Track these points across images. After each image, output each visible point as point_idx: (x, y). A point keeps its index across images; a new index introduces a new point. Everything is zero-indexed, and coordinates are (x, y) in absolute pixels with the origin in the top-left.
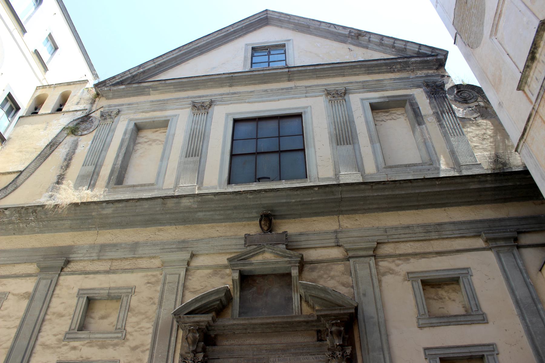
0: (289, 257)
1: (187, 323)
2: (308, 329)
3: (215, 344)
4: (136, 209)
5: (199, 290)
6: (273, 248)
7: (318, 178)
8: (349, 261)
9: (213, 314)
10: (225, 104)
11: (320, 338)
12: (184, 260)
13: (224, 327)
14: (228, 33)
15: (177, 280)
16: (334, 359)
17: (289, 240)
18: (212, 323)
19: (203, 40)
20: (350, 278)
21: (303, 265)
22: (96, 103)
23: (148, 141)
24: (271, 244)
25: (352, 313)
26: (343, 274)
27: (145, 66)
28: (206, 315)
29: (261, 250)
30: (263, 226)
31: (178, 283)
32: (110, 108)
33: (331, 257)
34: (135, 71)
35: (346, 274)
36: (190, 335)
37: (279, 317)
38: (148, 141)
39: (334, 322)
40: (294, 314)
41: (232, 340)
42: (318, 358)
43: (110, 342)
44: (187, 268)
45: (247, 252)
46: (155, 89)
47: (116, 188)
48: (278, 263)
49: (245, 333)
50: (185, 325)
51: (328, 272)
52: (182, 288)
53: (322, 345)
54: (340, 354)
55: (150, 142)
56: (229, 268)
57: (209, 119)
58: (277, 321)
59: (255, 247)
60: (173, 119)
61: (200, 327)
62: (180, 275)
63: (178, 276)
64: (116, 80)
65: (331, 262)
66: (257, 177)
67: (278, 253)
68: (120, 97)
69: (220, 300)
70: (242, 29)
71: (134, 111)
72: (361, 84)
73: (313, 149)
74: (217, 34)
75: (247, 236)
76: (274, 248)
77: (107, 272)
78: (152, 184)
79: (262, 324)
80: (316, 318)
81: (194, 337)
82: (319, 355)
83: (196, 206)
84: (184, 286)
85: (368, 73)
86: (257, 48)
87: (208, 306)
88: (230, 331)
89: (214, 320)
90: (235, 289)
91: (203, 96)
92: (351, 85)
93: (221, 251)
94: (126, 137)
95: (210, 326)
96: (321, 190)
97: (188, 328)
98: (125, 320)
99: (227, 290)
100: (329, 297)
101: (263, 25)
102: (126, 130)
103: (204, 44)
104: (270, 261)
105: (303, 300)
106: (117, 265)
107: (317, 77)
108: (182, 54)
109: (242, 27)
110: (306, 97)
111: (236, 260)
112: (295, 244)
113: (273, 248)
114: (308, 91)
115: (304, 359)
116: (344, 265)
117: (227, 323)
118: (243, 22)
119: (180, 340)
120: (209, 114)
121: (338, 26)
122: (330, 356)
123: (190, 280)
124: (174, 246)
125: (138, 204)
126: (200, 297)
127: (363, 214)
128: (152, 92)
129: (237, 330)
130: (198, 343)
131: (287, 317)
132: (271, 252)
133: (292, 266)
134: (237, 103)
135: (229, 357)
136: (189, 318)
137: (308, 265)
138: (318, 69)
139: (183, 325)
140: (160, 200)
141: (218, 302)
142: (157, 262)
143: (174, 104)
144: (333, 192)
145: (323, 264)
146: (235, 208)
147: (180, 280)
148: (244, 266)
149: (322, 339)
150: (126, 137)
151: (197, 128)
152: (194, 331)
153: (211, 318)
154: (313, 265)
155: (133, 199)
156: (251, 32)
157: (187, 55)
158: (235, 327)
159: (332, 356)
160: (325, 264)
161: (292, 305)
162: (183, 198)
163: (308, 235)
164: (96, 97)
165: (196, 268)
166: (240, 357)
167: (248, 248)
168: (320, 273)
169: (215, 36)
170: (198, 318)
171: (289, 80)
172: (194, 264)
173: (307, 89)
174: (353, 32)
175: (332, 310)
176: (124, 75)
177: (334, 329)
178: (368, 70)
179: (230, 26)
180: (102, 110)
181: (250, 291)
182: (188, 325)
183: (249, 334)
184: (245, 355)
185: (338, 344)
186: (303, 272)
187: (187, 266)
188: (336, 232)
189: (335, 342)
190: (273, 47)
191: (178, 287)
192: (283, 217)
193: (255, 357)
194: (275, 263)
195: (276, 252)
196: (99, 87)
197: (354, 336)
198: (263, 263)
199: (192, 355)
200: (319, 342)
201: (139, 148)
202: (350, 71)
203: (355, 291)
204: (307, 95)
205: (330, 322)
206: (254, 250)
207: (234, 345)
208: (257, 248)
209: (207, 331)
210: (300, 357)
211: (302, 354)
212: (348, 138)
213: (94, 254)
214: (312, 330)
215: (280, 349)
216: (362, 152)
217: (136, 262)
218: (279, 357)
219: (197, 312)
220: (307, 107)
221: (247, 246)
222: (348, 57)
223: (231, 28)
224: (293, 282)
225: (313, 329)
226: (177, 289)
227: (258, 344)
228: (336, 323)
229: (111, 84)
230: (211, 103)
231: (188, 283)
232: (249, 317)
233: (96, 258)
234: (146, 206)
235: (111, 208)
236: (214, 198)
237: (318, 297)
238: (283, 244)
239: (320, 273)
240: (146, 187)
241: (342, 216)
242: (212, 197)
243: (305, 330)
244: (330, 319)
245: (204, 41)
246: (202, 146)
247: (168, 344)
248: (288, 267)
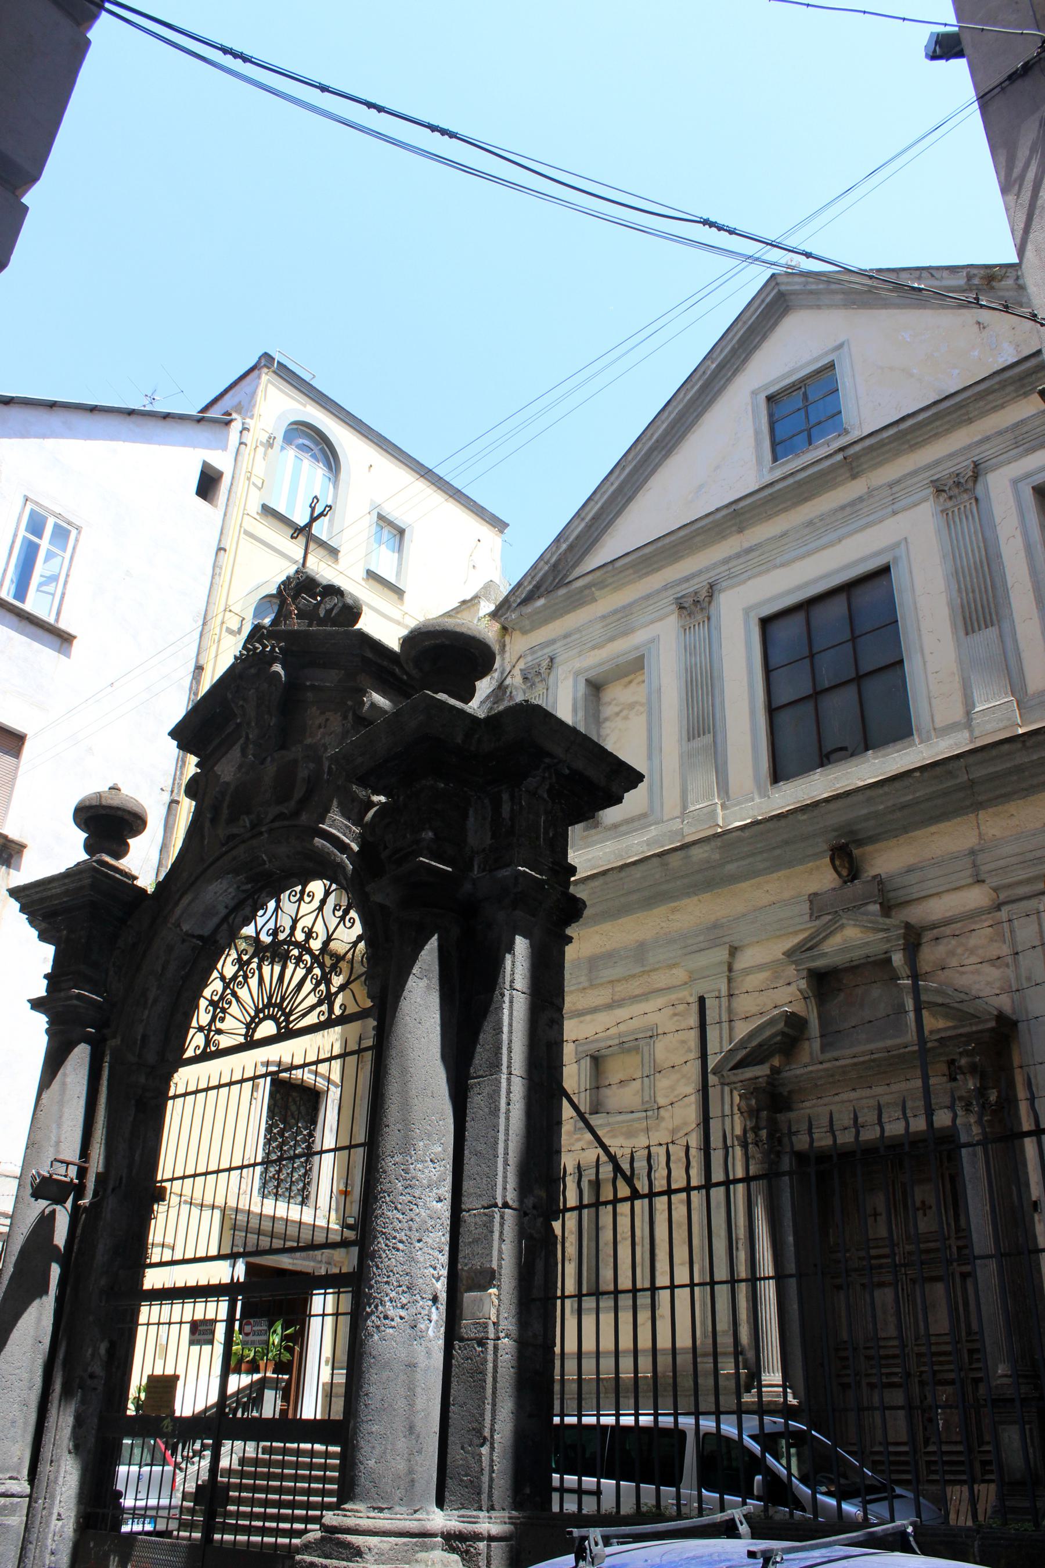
4: (623, 884)
7: (935, 729)
10: (740, 584)
12: (720, 963)
14: (707, 379)
19: (660, 422)
22: (507, 648)
23: (621, 711)
26: (992, 940)
27: (567, 533)
30: (840, 869)
32: (535, 656)
33: (968, 908)
34: (552, 555)
35: (996, 941)
38: (621, 711)
43: (637, 1125)
46: (601, 585)
47: (587, 837)
55: (625, 713)
57: (714, 632)
59: (830, 917)
60: (649, 649)
61: (758, 1086)
64: (524, 588)
66: (824, 752)
68: (546, 621)
69: (783, 1033)
70: (734, 352)
71: (579, 649)
72: (1009, 436)
73: (919, 655)
74: (683, 392)
75: (813, 898)
77: (609, 1007)
78: (644, 816)
81: (749, 1106)
83: (717, 856)
85: (1024, 393)
86: (779, 394)
91: (693, 576)
92: (987, 446)
93: (778, 933)
94: (578, 718)
96: (926, 774)
98: (652, 1087)
101: (779, 317)
102: (575, 700)
103: (665, 430)
106: (623, 990)
107: (911, 446)
108: (631, 474)
109: (733, 348)
110: (895, 513)
111: (798, 953)
112: (901, 892)
114: (897, 495)
118: (730, 336)
120: (713, 620)
121: (938, 268)
124: (701, 938)
125: (623, 874)
127: (1024, 798)
128: (597, 593)
132: (855, 925)
134: (760, 574)
138: (906, 429)
140: (655, 860)
142: (680, 975)
143: (645, 610)
144: (950, 772)
146: (786, 843)
150: (578, 718)
151: (696, 664)
155: (612, 869)
156: (756, 347)
157: (641, 471)
162: (693, 847)
163: (921, 869)
164: (503, 636)
169: (682, 400)
170: (749, 1073)
171: (854, 477)
172: (739, 965)
173: (895, 489)
174: (975, 276)
176: (536, 571)
178: (1023, 386)
179: (705, 358)
180: (521, 665)
181: (836, 1001)
188: (972, 852)
190: (810, 377)
192: (872, 840)
196: (502, 616)
198: (842, 950)
201: (608, 731)
202: (982, 403)
204: (896, 507)
212: (987, 610)
213: (583, 979)
216: (1019, 636)
217: (649, 980)
220: (896, 545)
222: (976, 353)
223: (709, 362)
229: (519, 600)
230: (712, 590)
233: (586, 984)
234: (638, 876)
235: (584, 890)
236: (742, 834)
238: (875, 902)
240: (636, 824)
241: (984, 812)
242: (739, 833)
245: (663, 422)
246: (713, 706)
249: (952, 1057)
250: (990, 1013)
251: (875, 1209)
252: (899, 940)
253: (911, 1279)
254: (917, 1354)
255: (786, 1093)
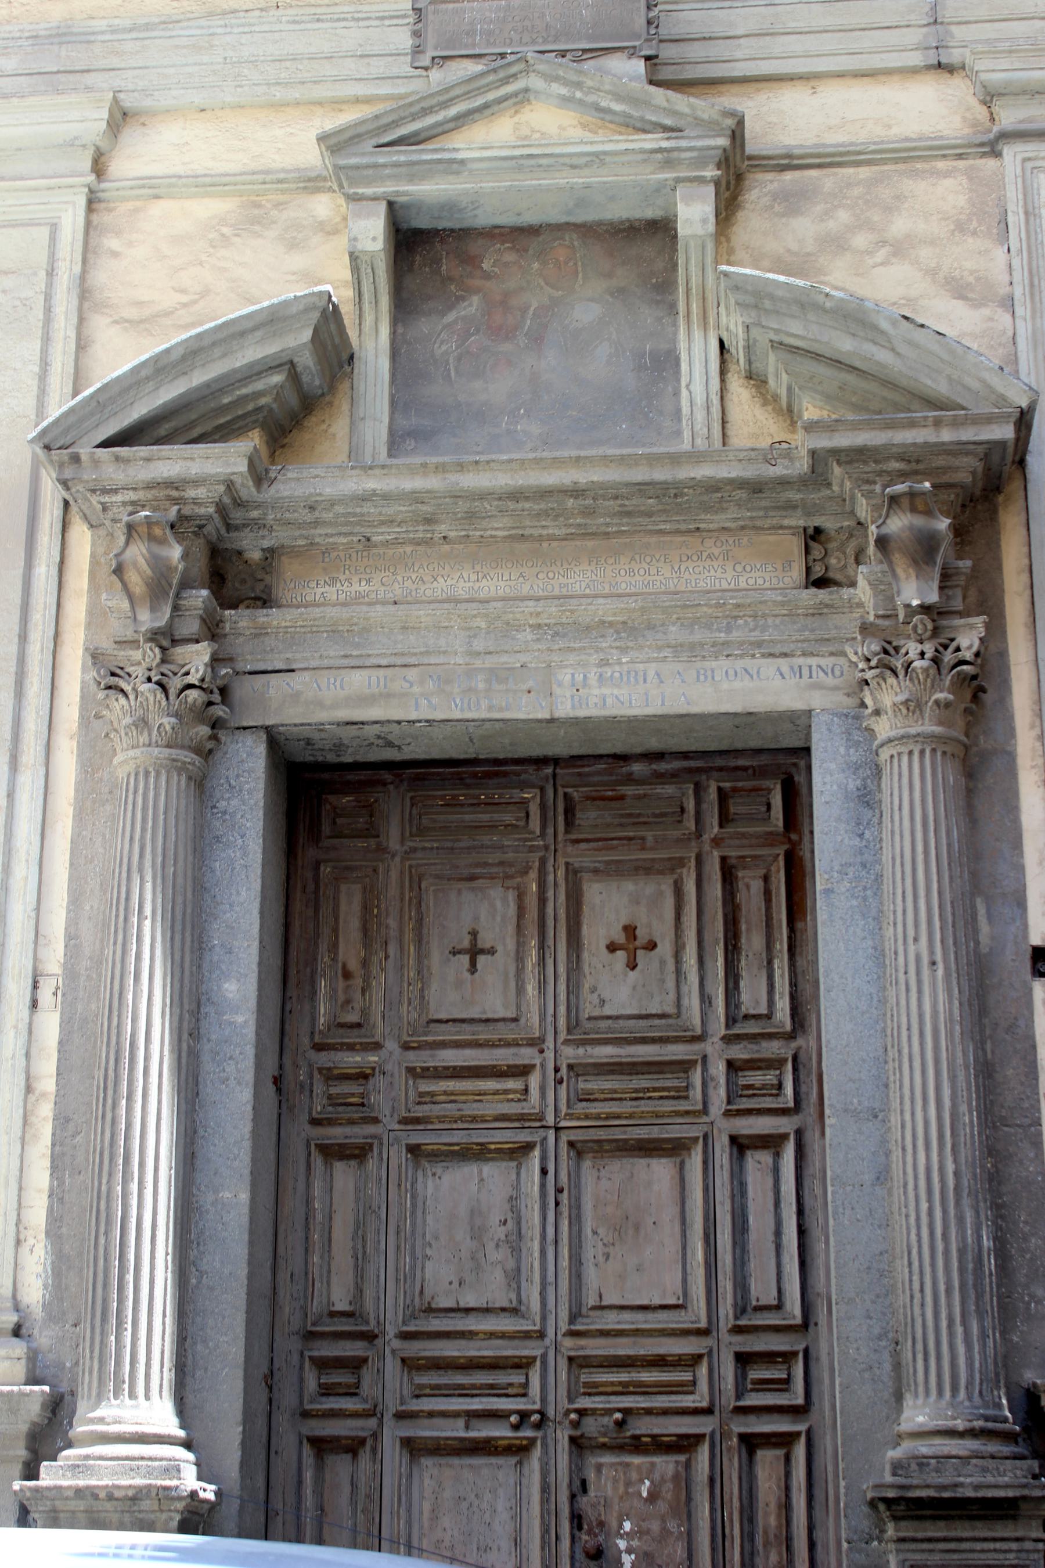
0: (666, 129)
1: (115, 491)
2: (759, 523)
3: (265, 601)
5: (168, 314)
6: (573, 77)
8: (997, 154)
9: (253, 441)
11: (818, 571)
12: (72, 144)
13: (312, 508)
15: (43, 259)
16: (892, 680)
17: (663, 32)
18: (247, 490)
20: (1000, 253)
21: (739, 177)
24: (563, 54)
25: (1002, 444)
26: (960, 227)
28: (216, 448)
29: (509, 89)
31: (51, 273)
33: (896, 131)
35: (974, 233)
36: (138, 553)
37: (606, 460)
39: (900, 488)
40: (686, 446)
41: (355, 579)
42: (805, 672)
44: (91, 191)
45: (432, 95)
48: (603, 163)
49: (427, 542)
50: (106, 499)
51: (876, 218)
52: (75, 302)
53: (827, 606)
54: (922, 654)
56: (330, 189)
58: (595, 479)
59: (474, 67)
61: (187, 511)
62: (54, 229)
63: (45, 231)
65: (896, 161)
67: (603, 104)
76: (581, 72)
79: (516, 495)
80: (802, 465)
82: (812, 654)
84: (84, 292)
87: (226, 401)
88: (344, 529)
89: (259, 477)
90: (366, 306)
93: (279, 93)
95: (239, 503)
97: (126, 519)
99: (324, 311)
100: (883, 356)
104: (557, 150)
105: (732, 367)
111: (368, 145)
112: (695, 51)
113: (573, 77)
115: (731, 672)
116: (970, 179)
117: (328, 491)
119: (79, 580)
122: (873, 663)
123: (115, 254)
126: (181, 351)
129: (383, 523)
130: (177, 596)
131: (653, 460)
132: (566, 101)
133: (678, 180)
135: (346, 662)
136: (127, 461)
137: (769, 176)
139: (94, 499)
141: (277, 379)
145: (850, 171)
147: (60, 255)
148: (411, 179)
149: (831, 574)
152: (157, 531)
153: (246, 462)
154: (797, 174)
158: (368, 508)
159: (881, 665)
160: (864, 172)
161: (677, 394)
165: (143, 187)
166: (399, 661)
167: (435, 75)
168: (831, 224)
175: (891, 425)
177: (898, 524)
181: (451, 317)
182: (119, 498)
183: (447, 547)
184: (427, 653)
185: (915, 603)
186: (740, 215)
187: (92, 178)
189: (899, 593)
191: (48, 297)
193: (478, 663)
194: (583, 160)
195: (591, 99)
197: (1000, 568)
199: (151, 655)
200: (813, 590)
203: (1020, 324)
205: (878, 488)
206: (471, 86)
207: (370, 604)
208: (482, 75)
209: (223, 531)
210: (714, 664)
211: (722, 649)
214: (781, 527)
215: (611, 624)
218: (604, 663)
219: (163, 430)
221: (427, 62)
224: (681, 270)
225: (786, 522)
226: (48, 310)
227: (495, 600)
228: (912, 495)
231: (101, 276)
232: (447, 459)
237: (817, 356)
238: (632, 52)
239: (831, 224)
243: (743, 528)
244: (880, 473)
247: (18, 601)
248: (658, 188)
249: (818, 521)
250: (1002, 399)
251: (474, 934)
252: (703, 168)
253: (571, 1144)
254: (571, 1359)
255: (256, 555)
